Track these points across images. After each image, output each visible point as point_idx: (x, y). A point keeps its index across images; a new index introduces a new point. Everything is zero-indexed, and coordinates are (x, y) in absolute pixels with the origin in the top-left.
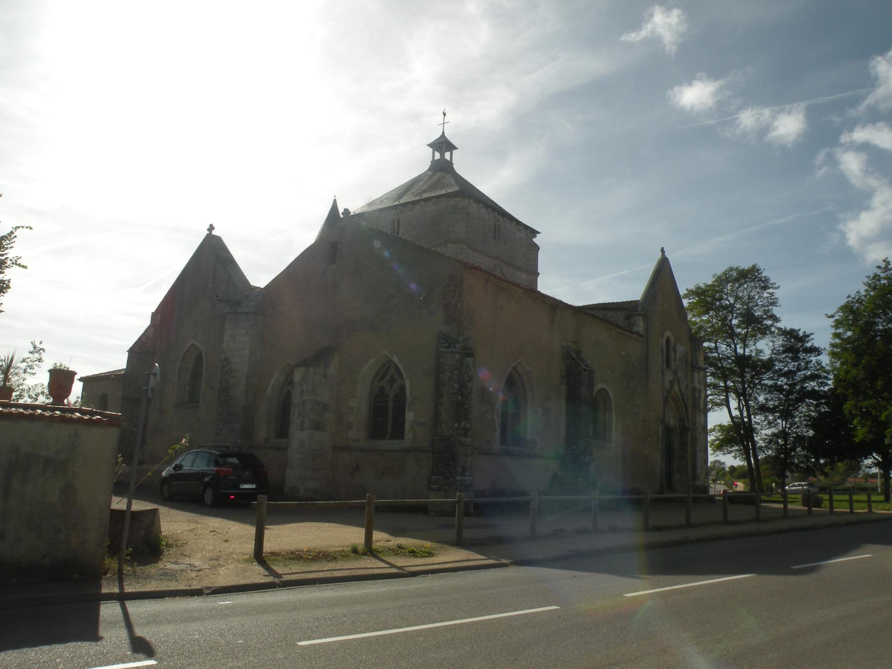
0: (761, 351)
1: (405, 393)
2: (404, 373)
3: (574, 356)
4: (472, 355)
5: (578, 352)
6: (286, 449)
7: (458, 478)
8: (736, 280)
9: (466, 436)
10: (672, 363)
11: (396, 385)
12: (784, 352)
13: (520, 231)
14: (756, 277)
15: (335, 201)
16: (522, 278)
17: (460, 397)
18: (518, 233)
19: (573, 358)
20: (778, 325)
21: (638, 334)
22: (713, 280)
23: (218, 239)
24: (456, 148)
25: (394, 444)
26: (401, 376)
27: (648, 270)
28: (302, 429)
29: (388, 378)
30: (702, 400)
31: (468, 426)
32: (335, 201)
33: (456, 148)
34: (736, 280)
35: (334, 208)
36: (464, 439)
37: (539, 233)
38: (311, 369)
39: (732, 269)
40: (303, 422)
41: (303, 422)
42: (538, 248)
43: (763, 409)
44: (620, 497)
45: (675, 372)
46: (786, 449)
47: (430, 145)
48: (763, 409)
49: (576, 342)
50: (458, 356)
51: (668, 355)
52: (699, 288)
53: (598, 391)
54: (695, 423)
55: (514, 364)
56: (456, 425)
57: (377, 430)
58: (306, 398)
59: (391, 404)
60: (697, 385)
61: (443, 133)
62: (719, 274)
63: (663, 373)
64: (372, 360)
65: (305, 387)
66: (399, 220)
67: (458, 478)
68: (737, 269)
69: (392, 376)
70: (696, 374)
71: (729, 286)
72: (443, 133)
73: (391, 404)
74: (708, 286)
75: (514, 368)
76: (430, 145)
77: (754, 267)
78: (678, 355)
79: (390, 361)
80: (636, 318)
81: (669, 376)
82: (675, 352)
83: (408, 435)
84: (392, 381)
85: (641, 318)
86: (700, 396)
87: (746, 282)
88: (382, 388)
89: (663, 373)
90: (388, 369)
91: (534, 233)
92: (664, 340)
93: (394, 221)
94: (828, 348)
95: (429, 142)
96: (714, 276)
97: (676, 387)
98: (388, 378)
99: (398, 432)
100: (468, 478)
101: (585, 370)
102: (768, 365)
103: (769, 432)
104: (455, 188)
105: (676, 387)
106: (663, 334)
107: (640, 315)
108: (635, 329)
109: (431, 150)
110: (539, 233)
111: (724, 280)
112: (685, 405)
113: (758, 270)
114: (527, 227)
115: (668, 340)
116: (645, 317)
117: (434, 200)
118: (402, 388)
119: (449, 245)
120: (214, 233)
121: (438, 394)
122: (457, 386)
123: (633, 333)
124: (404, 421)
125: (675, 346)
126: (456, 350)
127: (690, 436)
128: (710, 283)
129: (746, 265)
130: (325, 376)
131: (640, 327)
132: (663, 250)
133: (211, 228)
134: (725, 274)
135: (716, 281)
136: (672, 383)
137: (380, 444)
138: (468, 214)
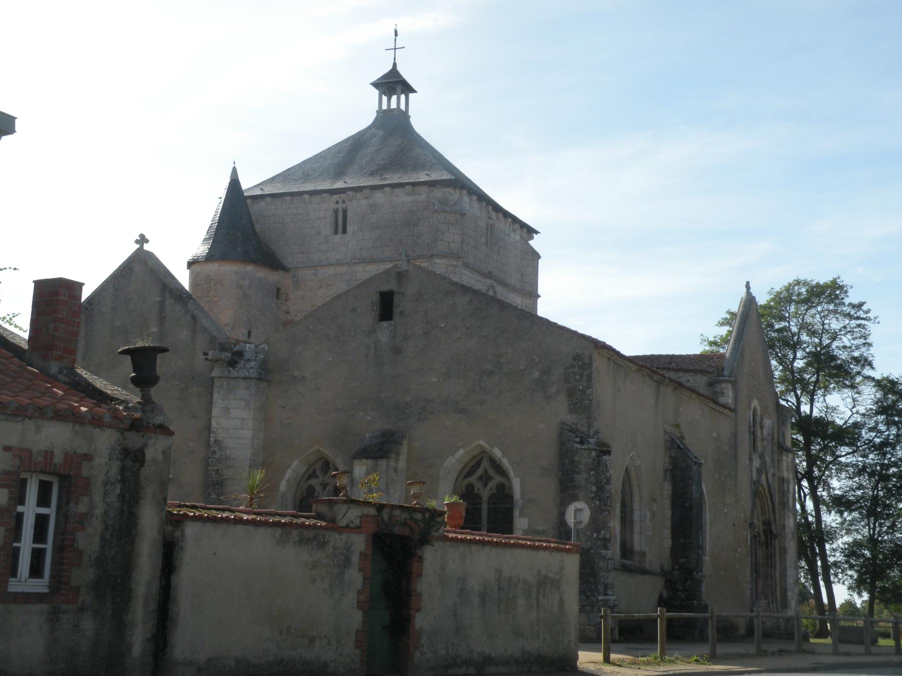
0: (834, 409)
4: (608, 453)
5: (682, 438)
7: (600, 598)
8: (806, 301)
9: (606, 548)
10: (759, 443)
11: (492, 484)
12: (878, 413)
13: (514, 231)
14: (837, 297)
15: (234, 171)
16: (517, 300)
17: (597, 502)
20: (867, 372)
21: (725, 406)
22: (768, 298)
23: (151, 256)
24: (413, 91)
29: (480, 472)
30: (791, 495)
31: (608, 536)
32: (234, 171)
33: (413, 91)
34: (806, 301)
35: (234, 184)
36: (604, 552)
37: (537, 232)
39: (798, 283)
42: (539, 257)
43: (840, 503)
45: (762, 457)
46: (875, 565)
47: (376, 85)
48: (840, 503)
50: (594, 454)
51: (754, 433)
54: (784, 526)
56: (595, 535)
59: (485, 507)
60: (785, 474)
61: (395, 65)
62: (778, 289)
63: (751, 459)
64: (461, 452)
66: (345, 212)
67: (600, 598)
68: (805, 283)
69: (486, 471)
70: (784, 458)
71: (793, 309)
72: (395, 65)
73: (485, 507)
76: (376, 85)
77: (834, 282)
78: (765, 433)
80: (723, 385)
81: (757, 463)
82: (762, 428)
84: (485, 479)
85: (730, 386)
86: (788, 488)
87: (820, 303)
89: (751, 459)
90: (478, 464)
91: (531, 232)
92: (751, 413)
93: (336, 211)
96: (769, 293)
97: (763, 477)
98: (480, 472)
100: (611, 598)
102: (847, 435)
103: (848, 539)
104: (446, 176)
105: (763, 477)
106: (750, 404)
107: (729, 382)
108: (722, 400)
109: (376, 92)
110: (537, 232)
111: (784, 298)
112: (773, 503)
113: (841, 288)
116: (734, 384)
119: (437, 261)
120: (146, 247)
122: (594, 489)
123: (717, 403)
127: (777, 547)
129: (823, 278)
131: (728, 398)
133: (142, 240)
134: (788, 289)
135: (773, 300)
136: (760, 472)
138: (463, 215)
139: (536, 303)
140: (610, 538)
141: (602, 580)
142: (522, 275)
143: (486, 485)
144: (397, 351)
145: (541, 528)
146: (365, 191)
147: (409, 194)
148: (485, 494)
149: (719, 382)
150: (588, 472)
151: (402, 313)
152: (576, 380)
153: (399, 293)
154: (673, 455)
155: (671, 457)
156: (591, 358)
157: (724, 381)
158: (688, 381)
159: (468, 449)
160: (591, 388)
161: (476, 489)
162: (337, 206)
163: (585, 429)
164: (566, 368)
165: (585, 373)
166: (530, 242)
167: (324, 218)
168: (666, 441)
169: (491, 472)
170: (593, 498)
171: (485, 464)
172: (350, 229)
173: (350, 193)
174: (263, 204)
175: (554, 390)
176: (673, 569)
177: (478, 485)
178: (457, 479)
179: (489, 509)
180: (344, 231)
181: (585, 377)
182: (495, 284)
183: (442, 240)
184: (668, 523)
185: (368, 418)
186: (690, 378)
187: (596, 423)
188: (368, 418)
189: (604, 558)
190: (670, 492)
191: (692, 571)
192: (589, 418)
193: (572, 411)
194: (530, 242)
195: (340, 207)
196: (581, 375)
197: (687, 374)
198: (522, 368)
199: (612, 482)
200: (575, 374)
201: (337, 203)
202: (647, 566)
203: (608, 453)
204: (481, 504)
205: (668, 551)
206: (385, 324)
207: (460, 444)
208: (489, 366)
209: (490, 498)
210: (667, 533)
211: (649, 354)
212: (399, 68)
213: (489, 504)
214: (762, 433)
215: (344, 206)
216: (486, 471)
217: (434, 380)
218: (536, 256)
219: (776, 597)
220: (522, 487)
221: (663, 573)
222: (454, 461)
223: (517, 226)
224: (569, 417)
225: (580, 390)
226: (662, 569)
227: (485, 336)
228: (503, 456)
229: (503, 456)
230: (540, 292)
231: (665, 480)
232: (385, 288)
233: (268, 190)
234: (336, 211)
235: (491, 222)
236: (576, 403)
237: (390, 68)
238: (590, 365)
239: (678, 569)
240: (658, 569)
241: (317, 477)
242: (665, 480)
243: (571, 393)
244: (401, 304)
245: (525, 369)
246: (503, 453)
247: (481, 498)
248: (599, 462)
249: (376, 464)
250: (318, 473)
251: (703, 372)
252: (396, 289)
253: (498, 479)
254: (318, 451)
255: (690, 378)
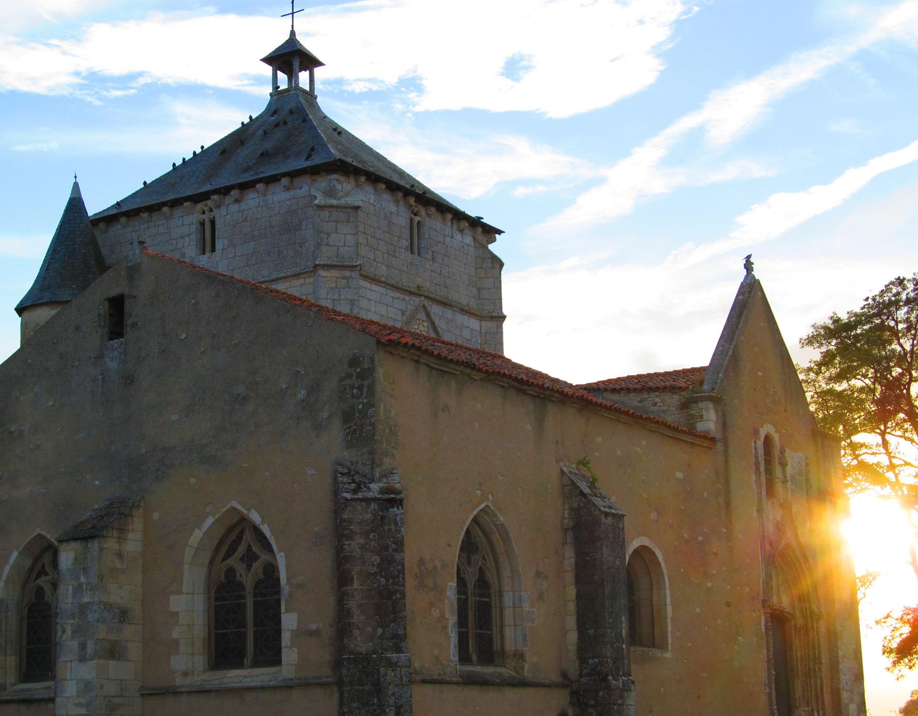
1: (278, 580)
2: (273, 542)
3: (587, 491)
4: (399, 503)
6: (52, 700)
9: (399, 650)
11: (257, 566)
13: (461, 231)
15: (76, 186)
18: (458, 236)
19: (582, 493)
24: (318, 63)
25: (261, 675)
26: (267, 546)
27: (726, 294)
28: (83, 659)
31: (401, 632)
32: (76, 186)
33: (318, 63)
35: (75, 205)
36: (394, 656)
37: (500, 232)
38: (95, 545)
40: (83, 646)
41: (83, 646)
42: (501, 265)
44: (82, 82)
47: (268, 60)
49: (583, 463)
52: (836, 321)
53: (636, 551)
55: (475, 513)
56: (380, 631)
57: (225, 650)
58: (86, 600)
59: (249, 602)
61: (293, 33)
65: (83, 579)
66: (213, 223)
69: (249, 548)
72: (293, 33)
73: (249, 602)
74: (856, 315)
75: (475, 520)
76: (268, 60)
78: (789, 469)
79: (244, 519)
80: (701, 405)
82: (783, 465)
83: (290, 655)
84: (249, 558)
88: (231, 571)
90: (240, 537)
91: (491, 232)
92: (760, 443)
94: (138, 694)
95: (262, 57)
98: (241, 549)
99: (270, 653)
101: (607, 515)
106: (756, 432)
108: (700, 427)
109: (268, 70)
110: (500, 232)
114: (476, 223)
115: (768, 440)
117: (285, 181)
118: (271, 570)
119: (323, 273)
121: (342, 578)
122: (376, 559)
124: (279, 632)
125: (782, 452)
126: (370, 495)
128: (858, 310)
130: (120, 555)
131: (709, 421)
132: (748, 266)
137: (234, 677)
139: (500, 328)
140: (405, 635)
141: (392, 701)
142: (479, 290)
143: (249, 567)
144: (129, 380)
145: (313, 627)
146: (233, 193)
147: (287, 189)
148: (248, 579)
149: (695, 401)
150: (366, 534)
151: (134, 325)
152: (353, 396)
153: (131, 296)
154: (575, 505)
155: (571, 509)
156: (372, 361)
157: (702, 399)
158: (655, 404)
159: (217, 516)
160: (373, 406)
161: (238, 575)
162: (203, 216)
163: (367, 470)
164: (341, 380)
165: (366, 383)
166: (491, 247)
167: (188, 235)
168: (563, 486)
169: (255, 548)
170: (375, 574)
171: (248, 536)
172: (219, 245)
173: (215, 197)
174: (119, 227)
175: (325, 415)
176: (581, 676)
177: (240, 568)
178: (212, 562)
179: (255, 603)
180: (213, 250)
181: (365, 390)
182: (427, 303)
183: (327, 245)
184: (572, 607)
185: (97, 482)
186: (657, 400)
187: (387, 460)
188: (97, 482)
189: (393, 665)
190: (573, 560)
191: (607, 675)
192: (372, 452)
193: (349, 445)
194: (491, 247)
195: (206, 217)
196: (360, 388)
197: (653, 395)
198: (284, 386)
199: (406, 548)
200: (353, 387)
201: (204, 213)
202: (527, 672)
203: (399, 503)
204: (244, 597)
205: (572, 648)
206: (115, 343)
207: (208, 510)
208: (241, 389)
209: (256, 587)
210: (571, 622)
211: (625, 375)
212: (298, 37)
213: (255, 596)
214: (784, 472)
215: (211, 215)
216: (249, 548)
217: (175, 417)
218: (498, 264)
219: (823, 702)
220: (288, 566)
221: (565, 682)
222: (199, 535)
223: (465, 224)
224: (345, 453)
225: (360, 411)
226: (564, 675)
227: (236, 345)
228: (263, 522)
229: (263, 522)
230: (505, 311)
231: (564, 543)
232: (113, 293)
233: (125, 209)
234: (202, 224)
235: (417, 219)
236: (355, 430)
237: (287, 37)
238: (372, 370)
239: (587, 675)
240: (555, 677)
241: (47, 574)
242: (564, 543)
243: (347, 417)
244: (134, 311)
245: (287, 388)
246: (262, 517)
247: (244, 589)
248: (383, 518)
249: (86, 547)
250: (47, 568)
251: (673, 389)
252: (126, 291)
253: (264, 557)
254: (40, 536)
255: (657, 400)
